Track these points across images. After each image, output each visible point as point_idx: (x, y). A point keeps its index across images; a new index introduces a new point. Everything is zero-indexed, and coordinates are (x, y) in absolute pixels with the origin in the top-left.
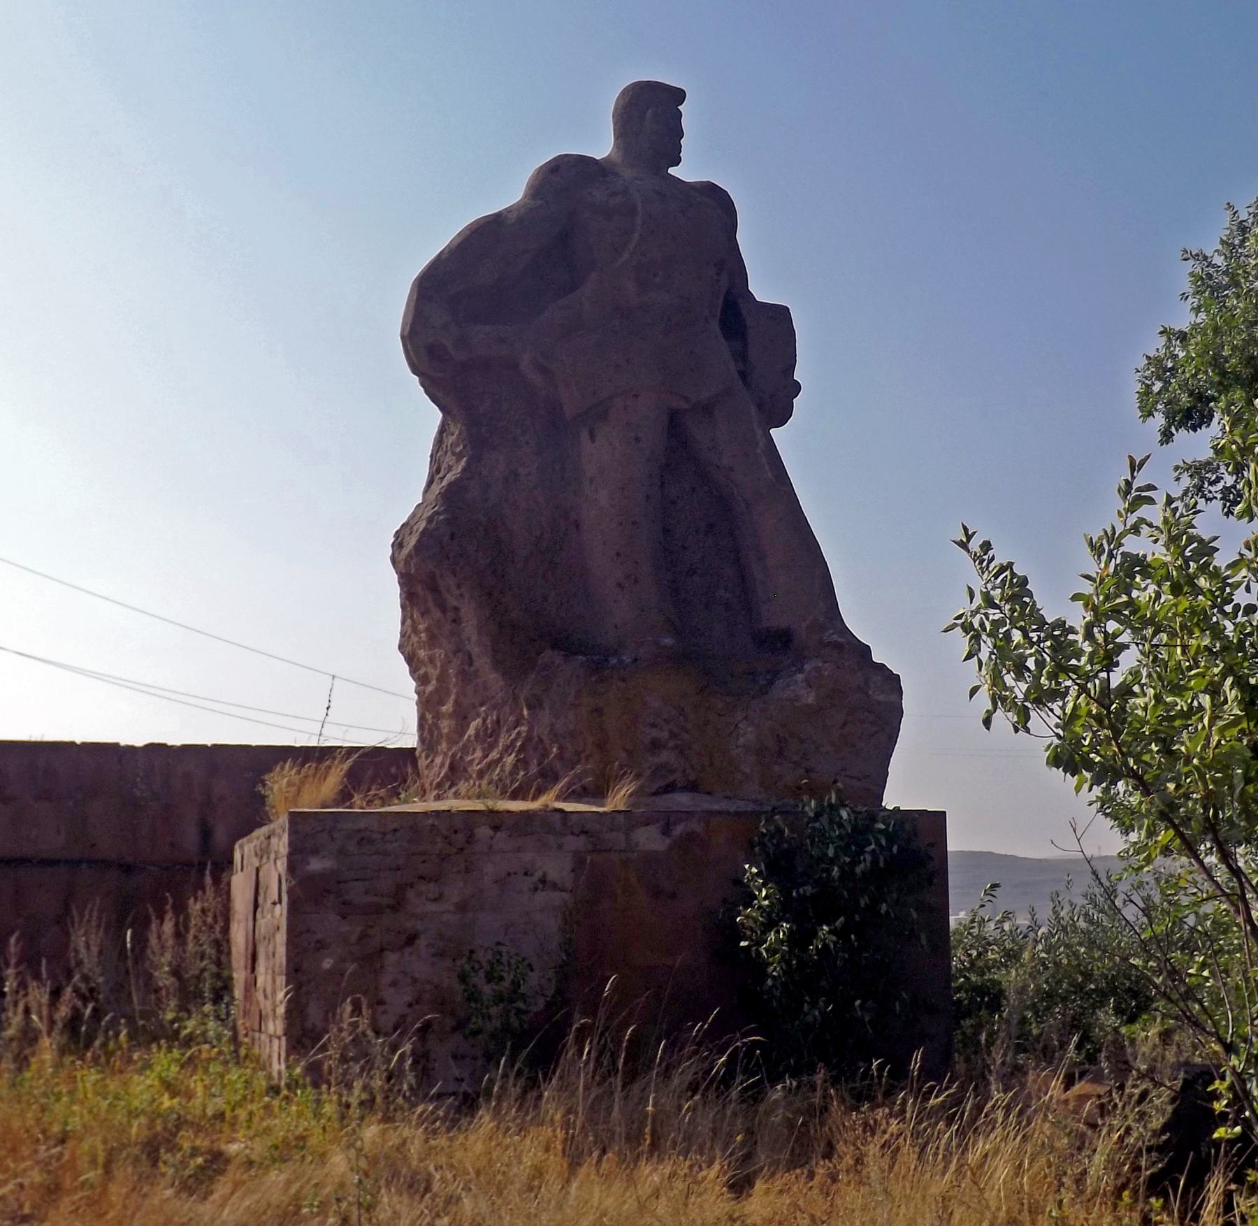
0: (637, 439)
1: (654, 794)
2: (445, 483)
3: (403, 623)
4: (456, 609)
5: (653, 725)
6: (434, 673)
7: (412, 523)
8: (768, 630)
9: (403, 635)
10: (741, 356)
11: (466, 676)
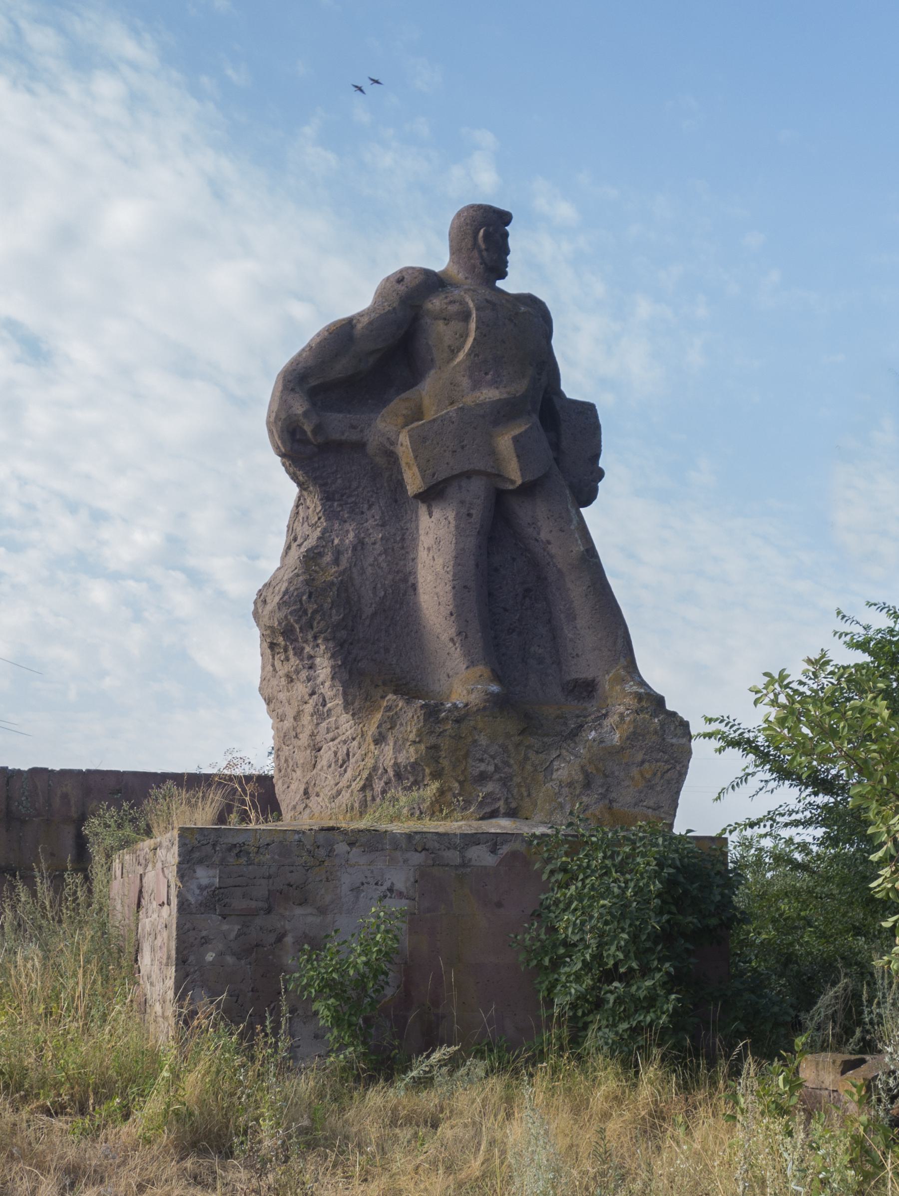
0: (469, 515)
1: (482, 819)
2: (303, 549)
3: (263, 668)
4: (311, 657)
5: (482, 760)
6: (290, 712)
7: (274, 583)
8: (576, 681)
9: (263, 679)
10: (556, 446)
11: (320, 715)
